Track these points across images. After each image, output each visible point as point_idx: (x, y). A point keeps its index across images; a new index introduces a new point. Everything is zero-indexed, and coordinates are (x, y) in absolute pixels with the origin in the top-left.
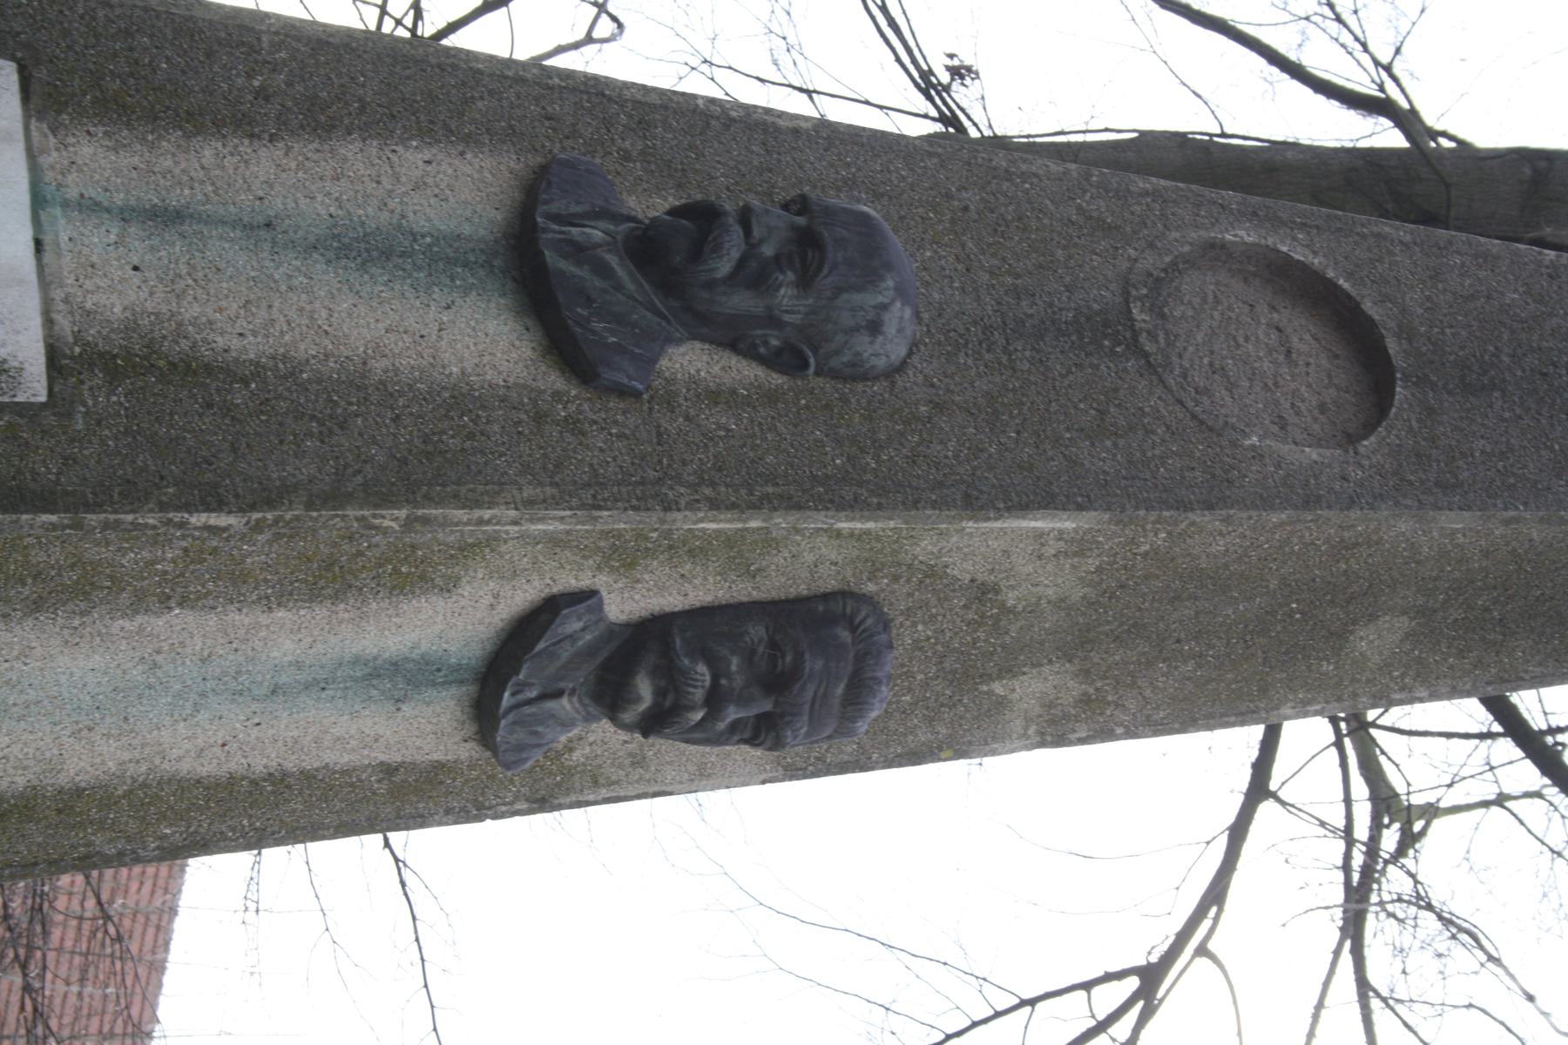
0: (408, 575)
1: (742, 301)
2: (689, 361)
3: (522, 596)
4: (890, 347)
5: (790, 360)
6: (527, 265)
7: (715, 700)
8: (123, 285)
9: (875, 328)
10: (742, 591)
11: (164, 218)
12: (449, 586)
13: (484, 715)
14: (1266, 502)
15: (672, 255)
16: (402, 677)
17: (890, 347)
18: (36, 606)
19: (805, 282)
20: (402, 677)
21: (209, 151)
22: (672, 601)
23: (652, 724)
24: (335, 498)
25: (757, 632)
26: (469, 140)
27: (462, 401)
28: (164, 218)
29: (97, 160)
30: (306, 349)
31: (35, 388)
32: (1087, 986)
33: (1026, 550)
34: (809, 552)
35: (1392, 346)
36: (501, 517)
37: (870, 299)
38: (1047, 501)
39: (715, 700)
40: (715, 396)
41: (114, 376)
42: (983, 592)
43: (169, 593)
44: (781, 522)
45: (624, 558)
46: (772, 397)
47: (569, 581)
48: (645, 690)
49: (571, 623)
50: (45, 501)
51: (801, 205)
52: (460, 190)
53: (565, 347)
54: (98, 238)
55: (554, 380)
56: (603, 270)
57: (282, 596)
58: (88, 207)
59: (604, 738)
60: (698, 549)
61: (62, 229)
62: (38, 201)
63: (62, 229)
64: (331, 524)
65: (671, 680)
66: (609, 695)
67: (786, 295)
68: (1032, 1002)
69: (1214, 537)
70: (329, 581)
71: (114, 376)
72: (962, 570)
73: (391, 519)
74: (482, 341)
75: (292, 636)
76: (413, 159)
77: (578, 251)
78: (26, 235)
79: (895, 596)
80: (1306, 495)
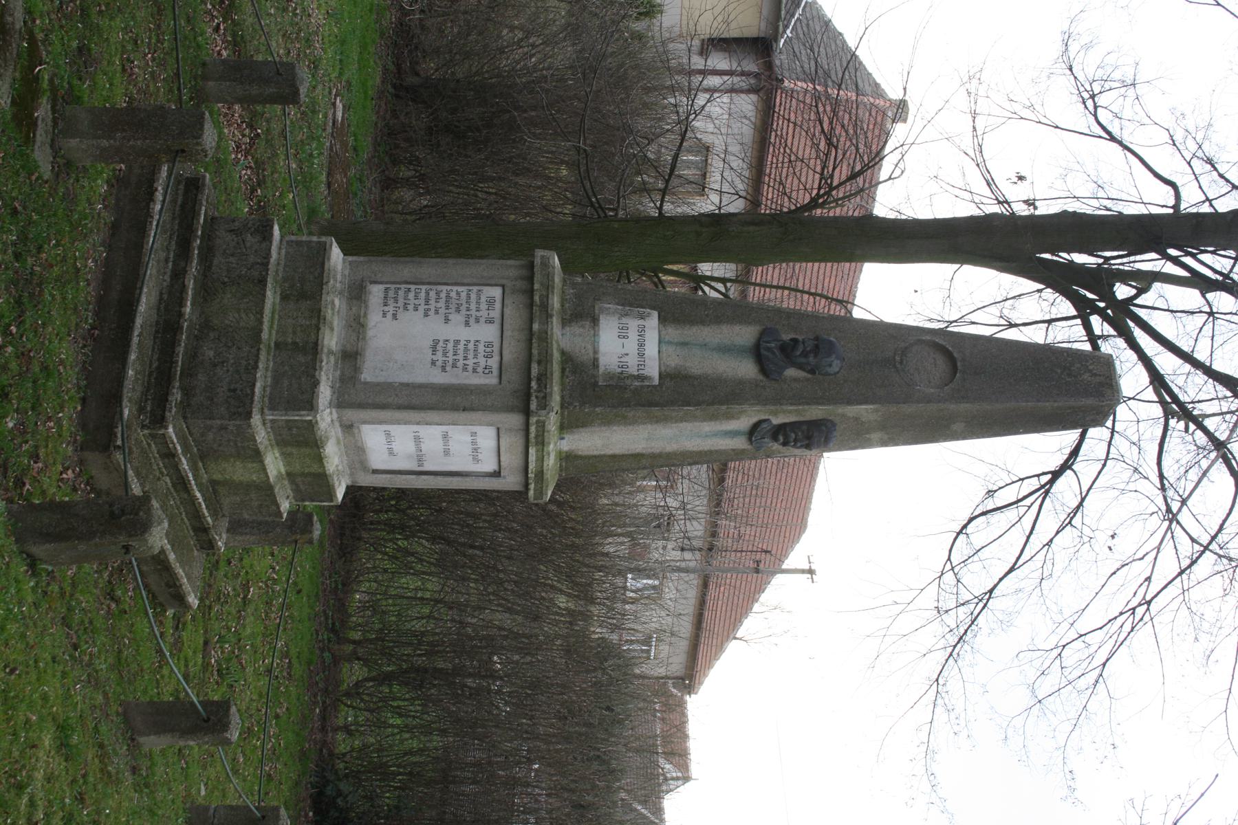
0: (729, 417)
1: (803, 360)
2: (791, 372)
3: (754, 420)
4: (835, 368)
5: (812, 372)
6: (758, 353)
7: (796, 441)
8: (675, 360)
9: (830, 365)
10: (802, 419)
11: (684, 344)
12: (738, 418)
13: (750, 440)
14: (918, 402)
15: (788, 350)
16: (733, 434)
17: (835, 368)
18: (657, 422)
19: (815, 356)
20: (733, 434)
21: (694, 329)
22: (787, 420)
23: (785, 444)
24: (712, 404)
25: (805, 427)
26: (750, 323)
27: (741, 382)
28: (684, 344)
29: (673, 332)
30: (710, 372)
31: (656, 382)
32: (1038, 476)
33: (864, 411)
34: (815, 412)
35: (959, 364)
36: (745, 407)
37: (829, 360)
38: (866, 403)
39: (796, 441)
40: (796, 380)
41: (672, 379)
42: (856, 419)
43: (682, 420)
44: (806, 407)
45: (775, 414)
46: (808, 380)
47: (763, 417)
48: (781, 438)
49: (764, 425)
50: (656, 405)
51: (817, 338)
52: (745, 334)
53: (763, 371)
54: (671, 349)
55: (761, 377)
56: (773, 353)
57: (704, 420)
58: (670, 343)
59: (776, 446)
60: (790, 412)
61: (664, 348)
62: (660, 342)
63: (664, 348)
64: (712, 409)
65: (786, 437)
66: (775, 438)
67: (811, 359)
68: (1022, 480)
69: (908, 409)
70: (713, 418)
71: (672, 379)
72: (851, 415)
73: (724, 407)
74: (746, 369)
75: (707, 427)
76: (737, 328)
77: (769, 349)
78: (657, 350)
79: (837, 420)
80: (929, 400)
